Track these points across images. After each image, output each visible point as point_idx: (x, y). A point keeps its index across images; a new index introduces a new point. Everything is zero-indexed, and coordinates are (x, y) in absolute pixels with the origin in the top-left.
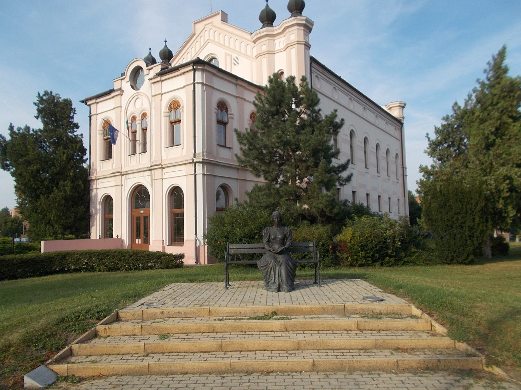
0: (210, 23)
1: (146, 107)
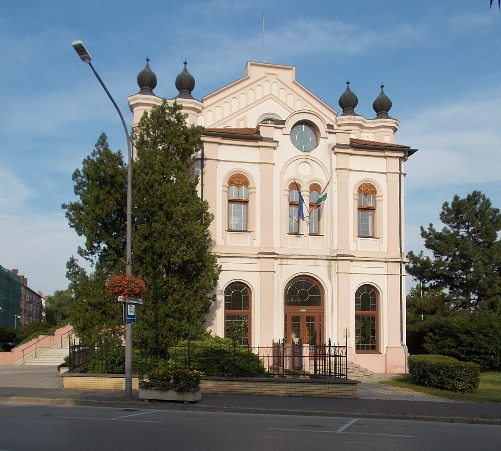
0: (275, 75)
1: (322, 179)
